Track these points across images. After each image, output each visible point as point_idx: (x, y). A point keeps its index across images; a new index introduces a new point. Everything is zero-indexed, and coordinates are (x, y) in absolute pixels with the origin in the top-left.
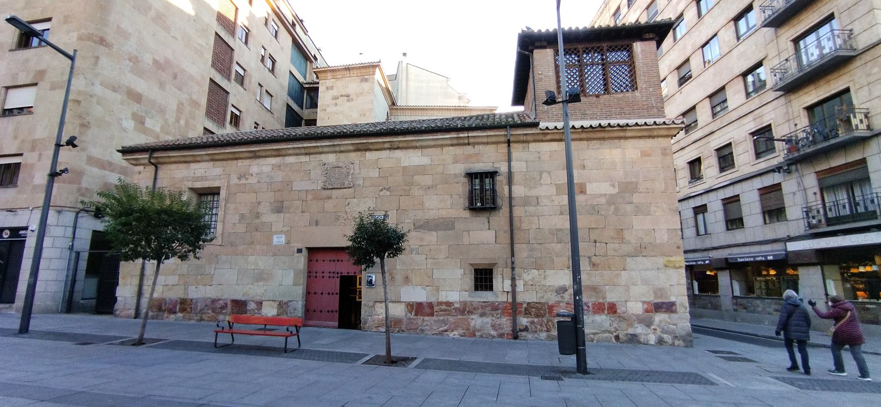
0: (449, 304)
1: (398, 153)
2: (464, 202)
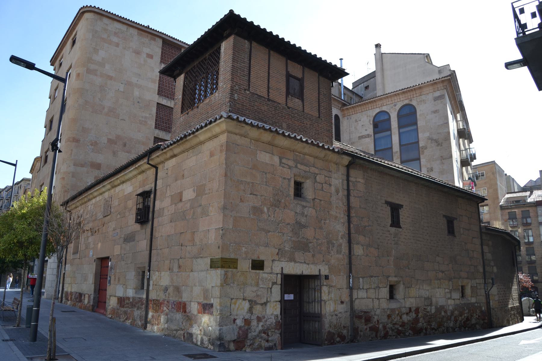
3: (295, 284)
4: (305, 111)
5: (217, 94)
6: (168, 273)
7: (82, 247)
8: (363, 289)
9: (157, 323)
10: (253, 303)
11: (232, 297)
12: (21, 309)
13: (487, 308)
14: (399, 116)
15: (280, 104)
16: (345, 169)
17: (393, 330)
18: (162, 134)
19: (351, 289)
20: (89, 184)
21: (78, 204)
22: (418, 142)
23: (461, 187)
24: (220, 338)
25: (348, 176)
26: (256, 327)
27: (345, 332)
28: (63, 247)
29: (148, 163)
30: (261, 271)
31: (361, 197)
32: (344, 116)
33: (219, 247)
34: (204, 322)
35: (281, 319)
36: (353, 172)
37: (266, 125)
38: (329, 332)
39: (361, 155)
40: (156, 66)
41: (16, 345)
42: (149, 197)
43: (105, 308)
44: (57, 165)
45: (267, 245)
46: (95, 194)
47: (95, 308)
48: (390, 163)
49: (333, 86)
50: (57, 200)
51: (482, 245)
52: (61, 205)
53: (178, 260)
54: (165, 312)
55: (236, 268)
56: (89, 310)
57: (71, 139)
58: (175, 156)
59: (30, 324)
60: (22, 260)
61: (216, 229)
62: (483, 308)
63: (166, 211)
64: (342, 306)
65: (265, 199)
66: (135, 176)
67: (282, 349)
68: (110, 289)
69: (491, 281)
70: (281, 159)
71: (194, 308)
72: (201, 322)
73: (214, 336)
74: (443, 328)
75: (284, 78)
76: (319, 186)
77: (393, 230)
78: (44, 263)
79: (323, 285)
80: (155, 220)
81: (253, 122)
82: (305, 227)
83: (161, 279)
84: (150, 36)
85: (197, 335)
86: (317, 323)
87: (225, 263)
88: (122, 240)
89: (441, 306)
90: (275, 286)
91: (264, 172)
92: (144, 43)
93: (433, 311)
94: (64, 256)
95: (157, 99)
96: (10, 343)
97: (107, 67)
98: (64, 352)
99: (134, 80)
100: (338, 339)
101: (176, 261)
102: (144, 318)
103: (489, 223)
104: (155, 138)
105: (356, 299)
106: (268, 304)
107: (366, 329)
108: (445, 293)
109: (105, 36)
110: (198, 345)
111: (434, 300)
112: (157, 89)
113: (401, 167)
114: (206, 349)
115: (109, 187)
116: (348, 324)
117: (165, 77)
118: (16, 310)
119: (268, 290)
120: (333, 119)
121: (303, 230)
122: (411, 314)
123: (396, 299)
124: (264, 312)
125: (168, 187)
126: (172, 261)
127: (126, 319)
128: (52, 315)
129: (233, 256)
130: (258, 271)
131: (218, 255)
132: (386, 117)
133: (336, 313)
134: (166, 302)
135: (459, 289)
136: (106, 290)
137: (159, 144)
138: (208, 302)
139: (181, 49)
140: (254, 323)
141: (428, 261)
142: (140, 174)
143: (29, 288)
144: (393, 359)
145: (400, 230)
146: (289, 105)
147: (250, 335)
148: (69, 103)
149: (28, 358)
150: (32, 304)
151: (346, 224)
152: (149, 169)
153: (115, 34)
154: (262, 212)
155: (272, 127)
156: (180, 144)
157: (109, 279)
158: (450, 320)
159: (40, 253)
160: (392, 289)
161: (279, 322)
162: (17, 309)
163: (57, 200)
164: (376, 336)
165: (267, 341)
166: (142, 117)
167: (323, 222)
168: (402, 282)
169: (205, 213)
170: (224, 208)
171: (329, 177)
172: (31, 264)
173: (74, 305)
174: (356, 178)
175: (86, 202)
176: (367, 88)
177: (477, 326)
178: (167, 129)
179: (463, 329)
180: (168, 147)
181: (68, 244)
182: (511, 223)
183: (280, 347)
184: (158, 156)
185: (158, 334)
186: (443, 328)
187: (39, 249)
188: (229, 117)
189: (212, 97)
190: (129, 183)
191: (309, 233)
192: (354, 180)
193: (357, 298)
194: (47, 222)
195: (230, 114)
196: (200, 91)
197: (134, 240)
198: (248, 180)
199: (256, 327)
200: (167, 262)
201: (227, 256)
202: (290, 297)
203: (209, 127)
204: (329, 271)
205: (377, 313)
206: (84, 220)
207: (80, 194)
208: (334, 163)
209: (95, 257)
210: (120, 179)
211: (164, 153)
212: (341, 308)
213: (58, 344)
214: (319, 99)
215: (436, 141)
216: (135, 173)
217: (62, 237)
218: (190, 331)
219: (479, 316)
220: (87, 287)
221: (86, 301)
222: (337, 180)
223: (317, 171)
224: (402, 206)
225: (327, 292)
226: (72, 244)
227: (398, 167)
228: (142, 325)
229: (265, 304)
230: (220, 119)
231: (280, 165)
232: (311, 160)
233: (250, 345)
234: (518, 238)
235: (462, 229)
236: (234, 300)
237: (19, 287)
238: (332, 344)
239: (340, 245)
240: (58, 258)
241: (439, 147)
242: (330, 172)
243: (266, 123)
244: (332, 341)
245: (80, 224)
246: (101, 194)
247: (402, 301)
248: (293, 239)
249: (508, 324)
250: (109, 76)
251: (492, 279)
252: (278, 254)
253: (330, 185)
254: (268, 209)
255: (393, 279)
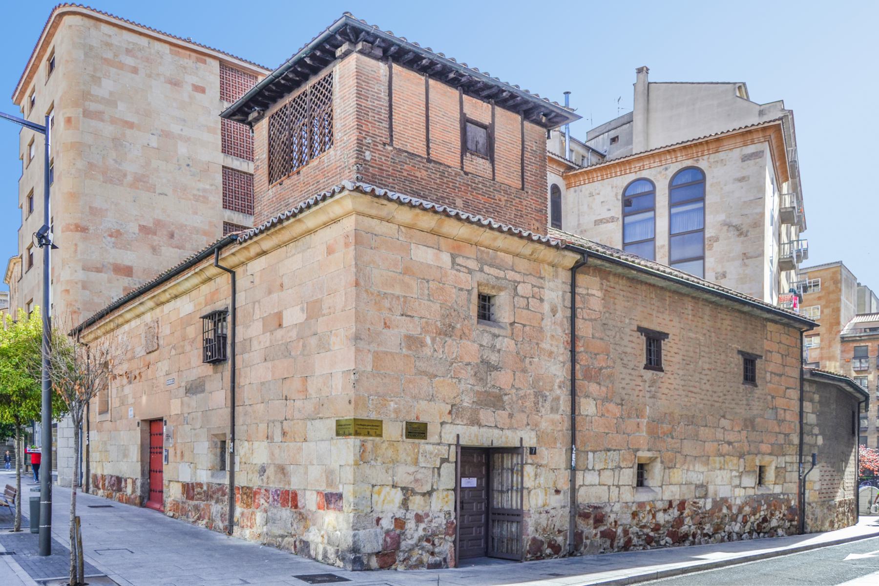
3: (482, 462)
4: (497, 179)
5: (332, 152)
6: (266, 443)
7: (114, 402)
8: (593, 469)
9: (249, 524)
10: (408, 492)
11: (374, 482)
12: (19, 504)
13: (800, 502)
14: (673, 187)
15: (449, 167)
16: (569, 273)
17: (639, 537)
18: (237, 218)
19: (573, 470)
20: (115, 299)
21: (99, 332)
22: (703, 230)
23: (775, 304)
24: (355, 549)
25: (573, 285)
26: (414, 532)
27: (560, 539)
28: (80, 402)
29: (217, 266)
30: (423, 441)
31: (595, 320)
32: (569, 186)
33: (350, 402)
34: (329, 524)
35: (456, 518)
36: (581, 279)
37: (424, 203)
38: (534, 540)
39: (597, 251)
40: (212, 107)
41: (17, 561)
42: (224, 319)
43: (161, 502)
44: (53, 269)
45: (432, 399)
46: (128, 316)
47: (146, 500)
48: (649, 264)
49: (549, 137)
50: (61, 326)
51: (801, 400)
52: (69, 335)
53: (282, 423)
54: (263, 507)
55: (380, 435)
56: (135, 504)
57: (72, 227)
59: (38, 528)
60: (12, 425)
61: (343, 372)
62: (793, 503)
63: (255, 343)
64: (558, 497)
65: (427, 323)
66: (196, 287)
67: (456, 566)
68: (168, 471)
69: (810, 459)
70: (453, 257)
71: (310, 501)
72: (323, 523)
73: (344, 546)
74: (723, 534)
75: (457, 125)
76: (523, 302)
77: (649, 374)
78: (50, 428)
79: (527, 463)
80: (237, 358)
81: (402, 197)
82: (496, 368)
83: (253, 454)
84: (194, 55)
85: (317, 544)
86: (515, 525)
87: (364, 428)
88: (183, 390)
89: (722, 499)
90: (445, 465)
91: (424, 279)
92: (185, 68)
93: (709, 506)
94: (84, 416)
95: (222, 160)
96: (8, 558)
97: (121, 106)
98: (98, 572)
99: (175, 128)
100: (548, 551)
101: (278, 425)
102: (227, 517)
103: (817, 364)
104: (225, 223)
105: (580, 486)
106: (435, 494)
107: (596, 535)
108: (731, 478)
109: (109, 55)
110: (318, 561)
111: (711, 489)
112: (220, 143)
113: (668, 270)
114: (332, 567)
115: (151, 304)
116: (567, 526)
117: (232, 123)
118: (11, 505)
119: (433, 472)
120: (549, 191)
121: (493, 373)
122: (671, 511)
123: (647, 487)
124: (428, 508)
125: (257, 304)
126: (271, 424)
127: (199, 519)
128: (74, 512)
129: (374, 416)
130: (417, 441)
131: (349, 414)
132: (648, 188)
133: (547, 508)
134: (263, 491)
135: (755, 471)
136: (161, 472)
137: (234, 233)
138: (334, 491)
139: (256, 78)
140: (411, 525)
141: (706, 426)
142: (204, 282)
143: (30, 469)
144: (635, 582)
145: (662, 374)
146: (466, 169)
147: (403, 544)
148: (59, 167)
149: (39, 582)
150: (38, 494)
151: (569, 365)
152: (219, 274)
153: (128, 51)
154: (422, 344)
155: (436, 206)
156: (272, 234)
157: (164, 453)
158: (736, 521)
159: (43, 412)
160: (642, 470)
161: (452, 523)
162: (13, 503)
163: (62, 327)
164: (612, 546)
165: (432, 554)
166: (198, 190)
167: (527, 360)
168: (659, 460)
169: (323, 346)
170: (357, 338)
171: (539, 287)
172: (29, 430)
173: (109, 496)
174: (588, 289)
175: (113, 330)
176: (614, 140)
177: (780, 531)
178: (248, 209)
179: (755, 535)
180: (251, 238)
181: (90, 398)
182: (858, 364)
183: (453, 564)
184: (233, 254)
185: (253, 542)
186: (723, 534)
187: (39, 405)
188: (357, 189)
189: (324, 157)
190: (185, 298)
191: (503, 379)
192: (584, 292)
193: (583, 485)
194: (48, 363)
195: (358, 184)
196: (301, 146)
197: (203, 391)
198: (398, 291)
199: (414, 532)
200: (262, 426)
201: (363, 415)
202: (471, 482)
203: (321, 205)
204: (538, 440)
205: (614, 509)
206: (113, 358)
207: (101, 316)
208: (549, 264)
209: (138, 419)
210: (170, 291)
211: (244, 248)
212: (556, 501)
213: (87, 559)
214: (522, 160)
215: (737, 228)
216: (196, 280)
217: (77, 387)
218: (305, 538)
219: (784, 515)
220: (130, 467)
221: (129, 490)
222: (555, 292)
223: (518, 277)
224: (666, 335)
225: (532, 474)
226: (97, 398)
227: (664, 272)
228: (226, 528)
229: (429, 493)
230: (340, 192)
231: (453, 267)
232: (509, 259)
233: (404, 560)
234: (866, 390)
235: (768, 375)
236: (376, 488)
237: (13, 468)
238: (538, 558)
239: (558, 399)
240: (74, 421)
241: (742, 238)
242: (542, 278)
243: (424, 197)
244: (539, 554)
245: (106, 365)
246: (138, 316)
247: (658, 490)
248: (476, 388)
249: (832, 527)
250: (126, 122)
251: (813, 456)
252: (450, 413)
253: (542, 300)
254: (433, 340)
255: (644, 455)
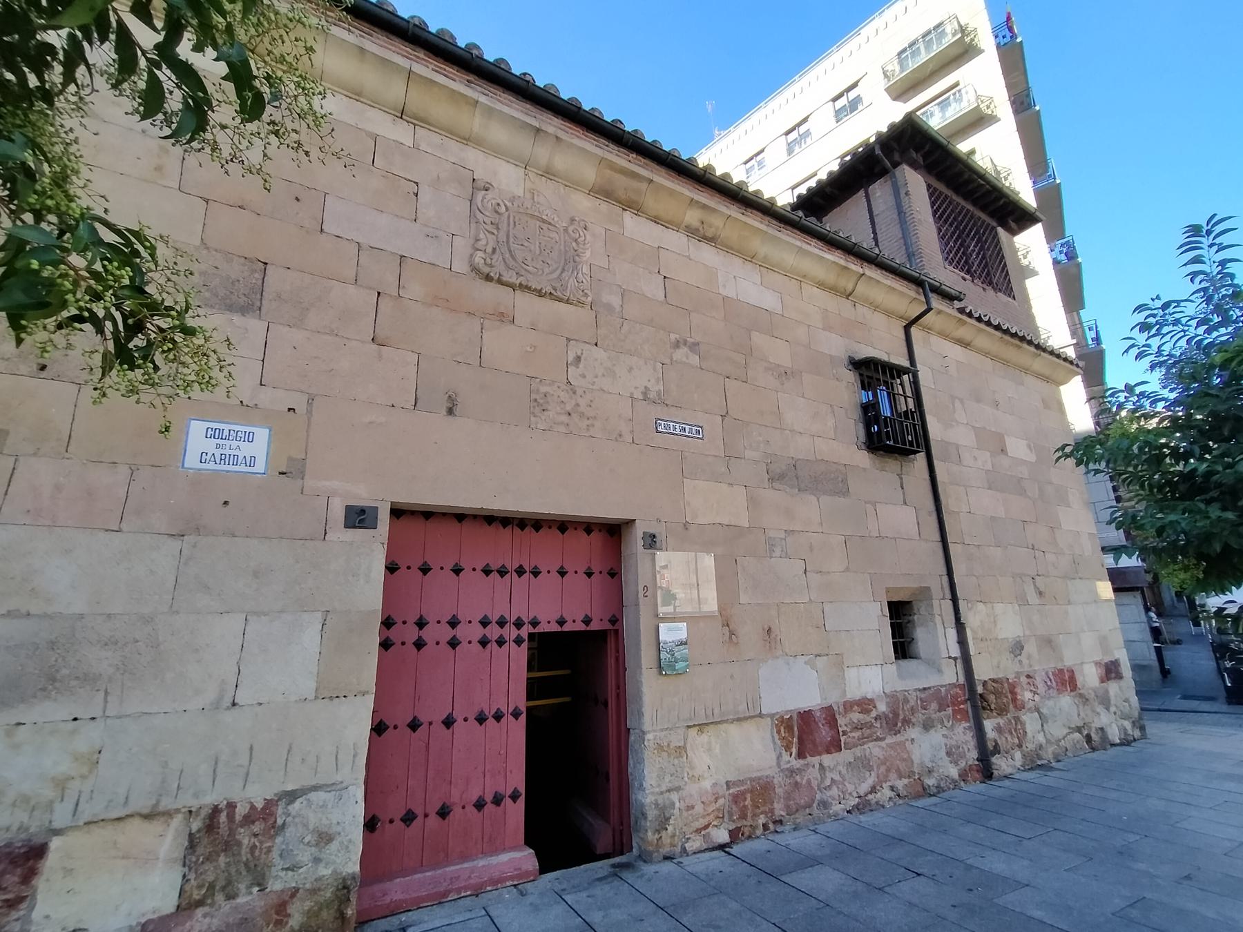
0: (865, 705)
1: (707, 254)
2: (854, 429)
58: (965, 344)
216: (395, 90)
249: (543, 706)
